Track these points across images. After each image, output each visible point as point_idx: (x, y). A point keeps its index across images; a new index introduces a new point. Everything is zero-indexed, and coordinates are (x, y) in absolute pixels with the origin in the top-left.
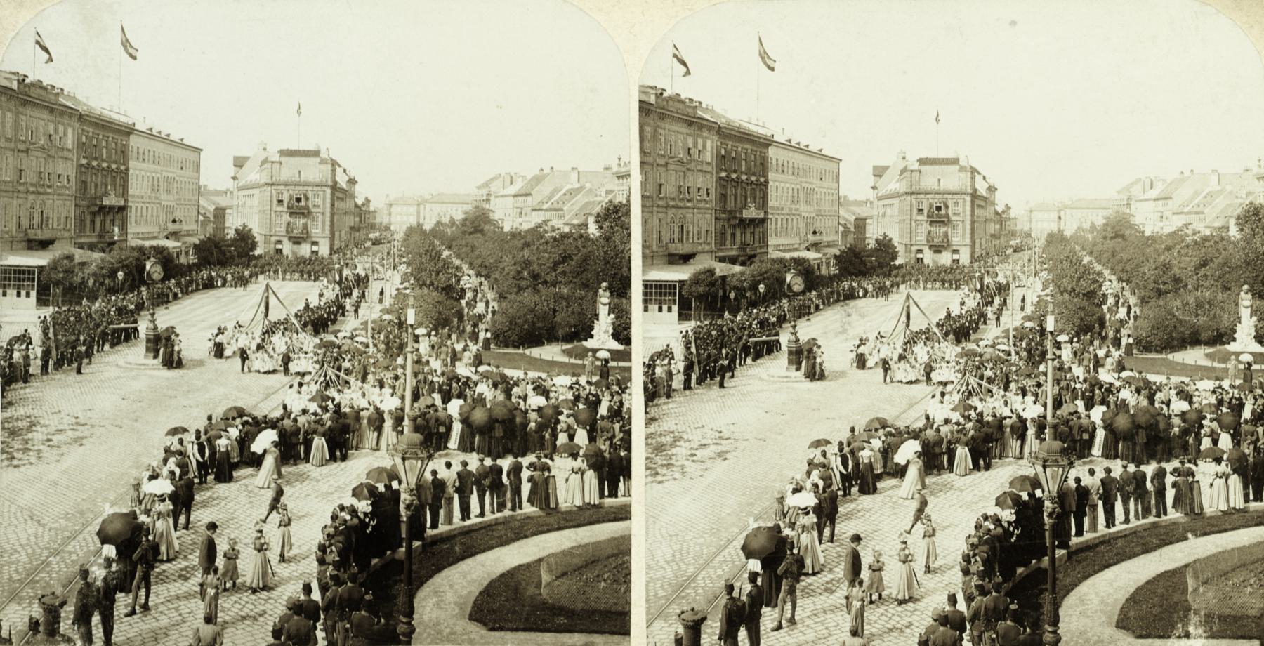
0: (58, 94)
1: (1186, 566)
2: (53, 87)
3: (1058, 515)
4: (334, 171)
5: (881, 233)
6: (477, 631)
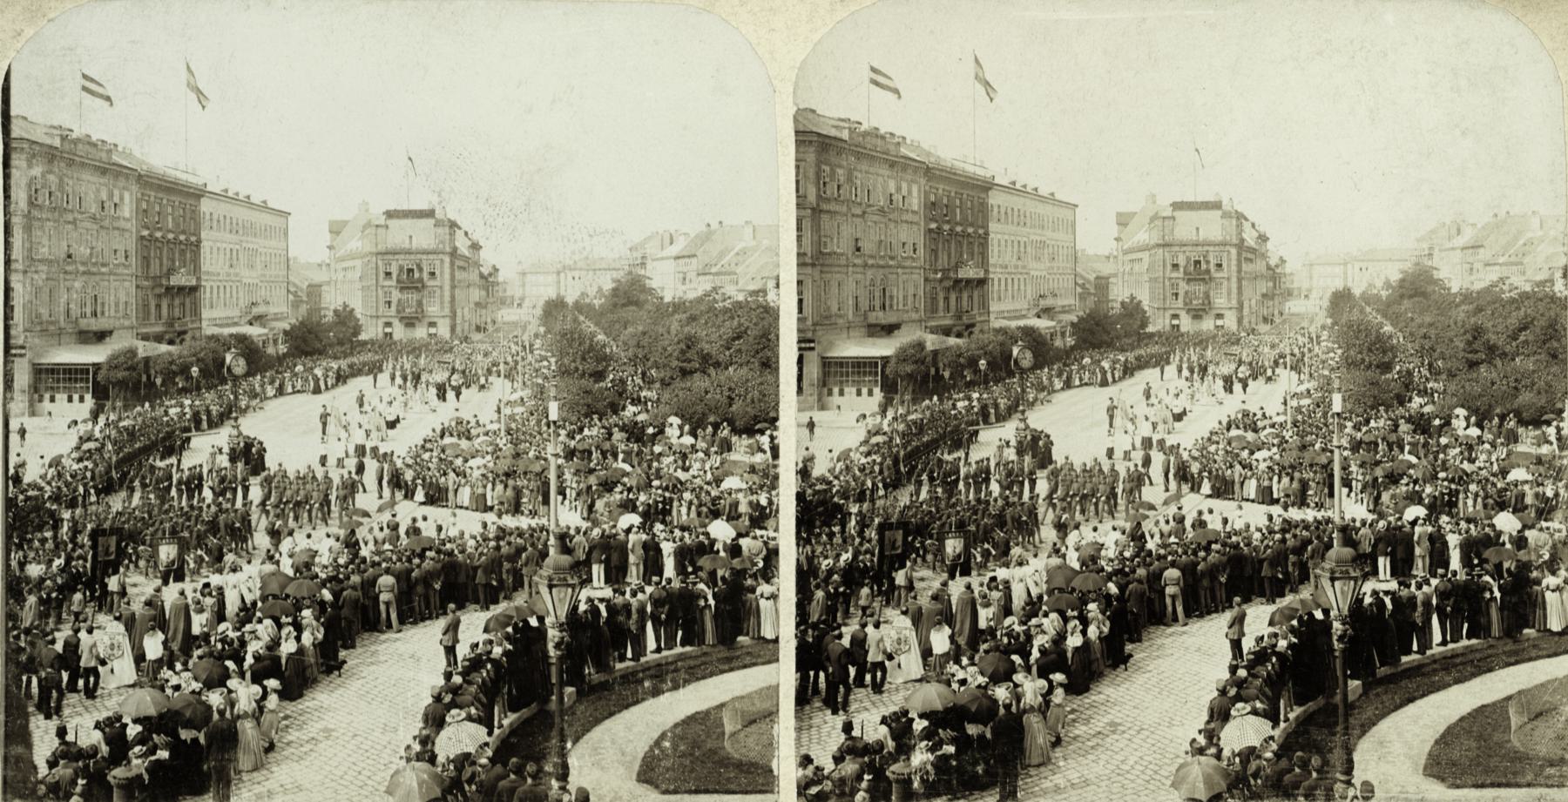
0: (899, 143)
1: (1509, 698)
2: (892, 135)
3: (1351, 638)
4: (1239, 226)
5: (340, 302)
6: (1436, 789)
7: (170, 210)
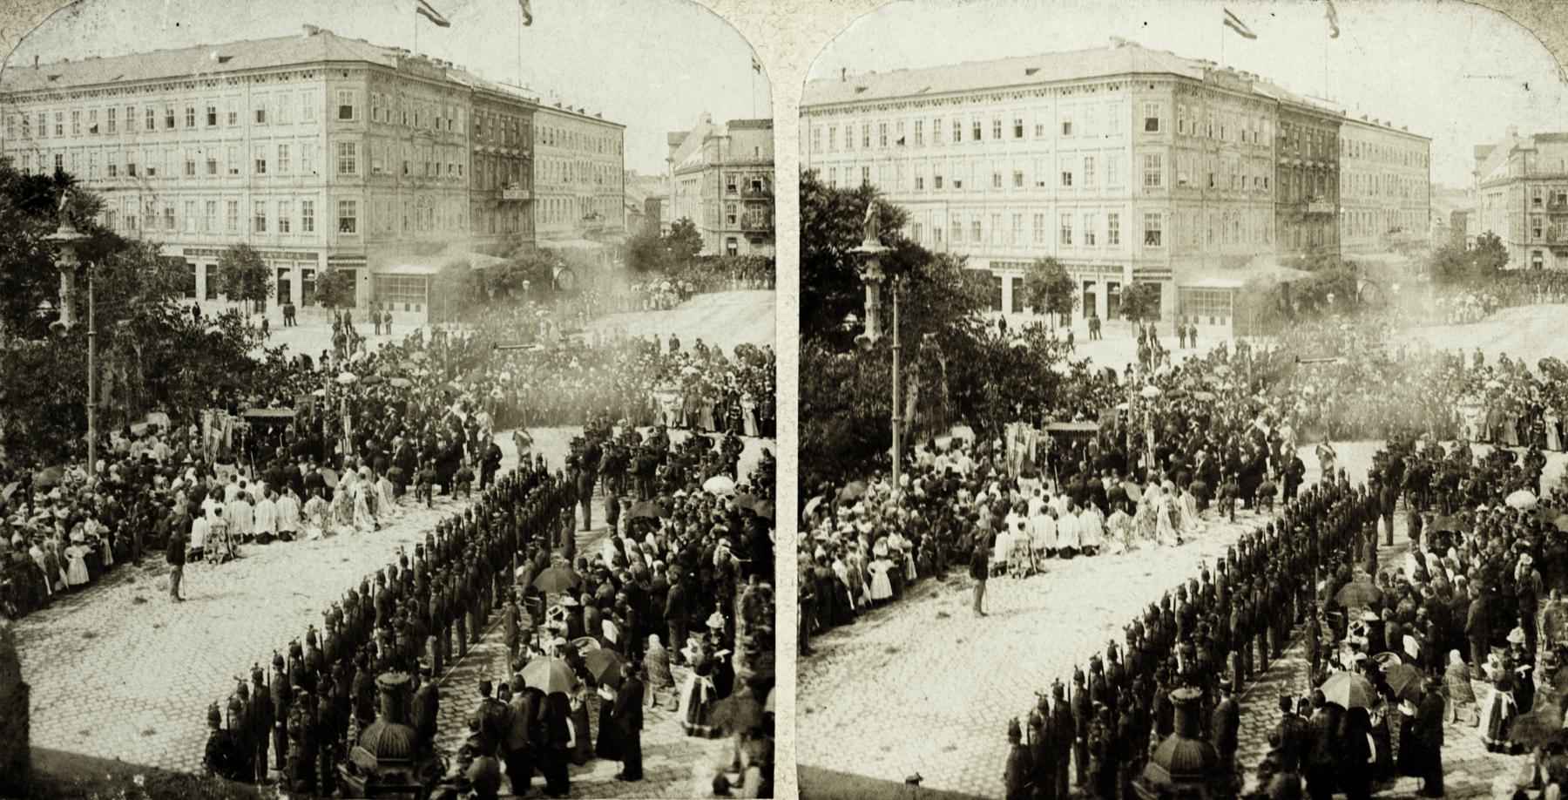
0: (445, 69)
5: (1485, 230)
7: (1309, 139)
